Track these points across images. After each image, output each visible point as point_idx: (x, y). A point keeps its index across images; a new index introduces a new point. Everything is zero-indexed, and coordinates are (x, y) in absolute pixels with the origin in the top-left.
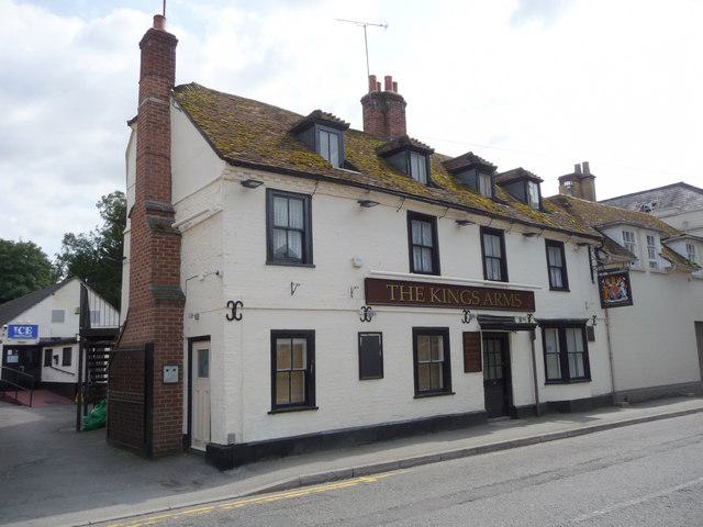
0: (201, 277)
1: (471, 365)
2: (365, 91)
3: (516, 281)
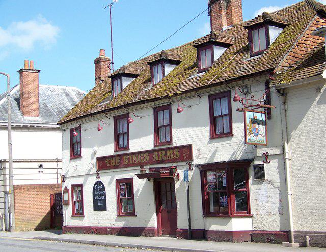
3: (180, 137)
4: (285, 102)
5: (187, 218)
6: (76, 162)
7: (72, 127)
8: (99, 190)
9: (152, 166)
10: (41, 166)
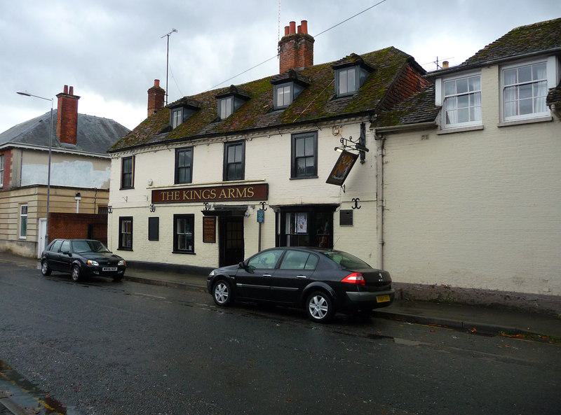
0: (123, 293)
1: (208, 238)
2: (152, 85)
3: (253, 174)
4: (383, 147)
5: (384, 235)
6: (127, 192)
7: (178, 146)
8: (154, 224)
9: (217, 203)
10: (78, 195)
